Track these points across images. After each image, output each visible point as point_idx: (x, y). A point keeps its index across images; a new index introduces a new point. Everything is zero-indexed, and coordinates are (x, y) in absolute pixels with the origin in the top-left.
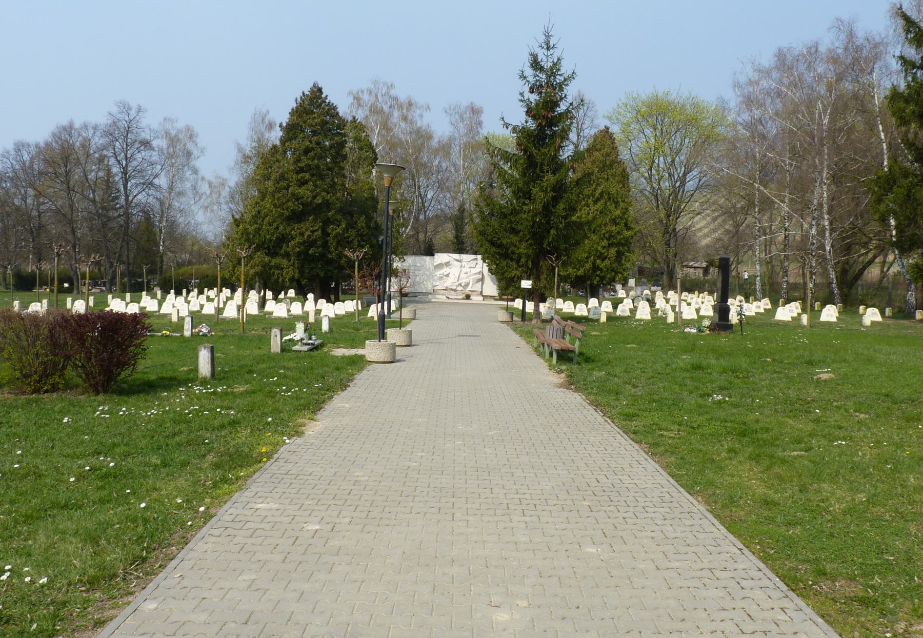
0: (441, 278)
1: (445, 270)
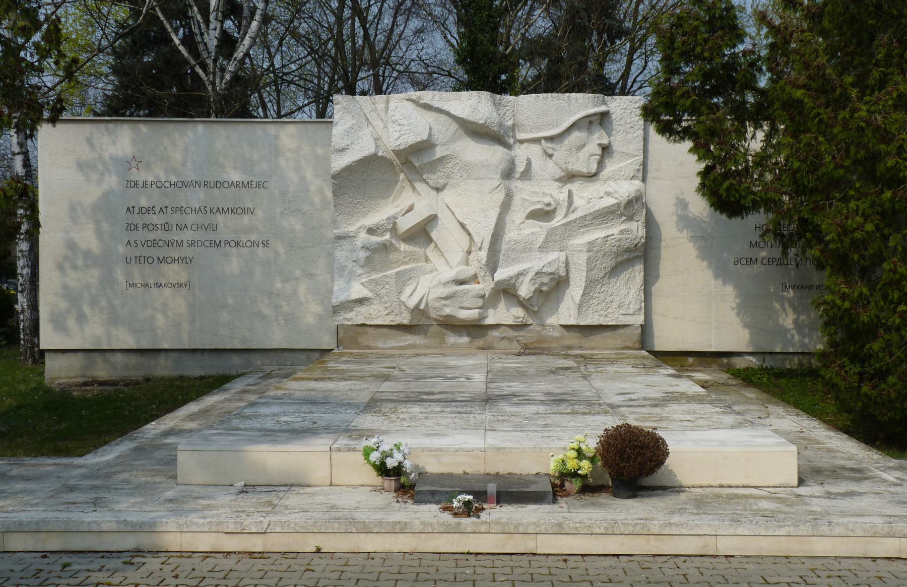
0: (378, 255)
1: (408, 203)
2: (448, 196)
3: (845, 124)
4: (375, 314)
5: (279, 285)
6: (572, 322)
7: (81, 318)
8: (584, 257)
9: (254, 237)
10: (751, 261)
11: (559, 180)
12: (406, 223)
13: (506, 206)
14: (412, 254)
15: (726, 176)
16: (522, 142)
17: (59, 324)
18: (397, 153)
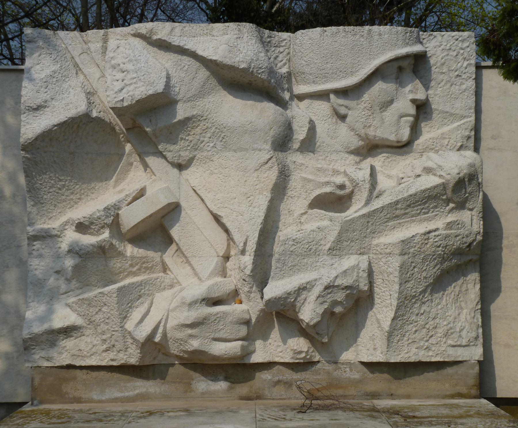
0: (91, 265)
1: (138, 186)
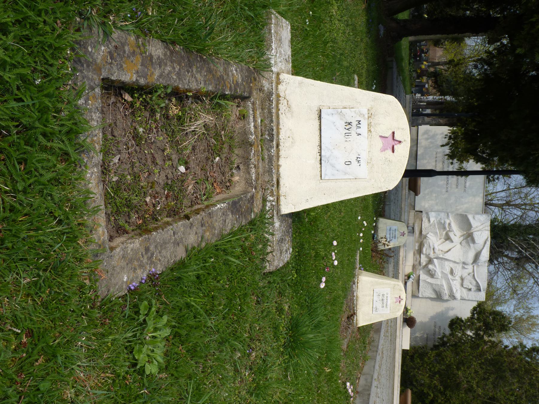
0: (442, 226)
1: (457, 234)
2: (459, 246)
3: (472, 359)
4: (425, 224)
5: (434, 195)
6: (421, 278)
7: (427, 139)
8: (439, 283)
9: (449, 188)
10: (435, 326)
11: (462, 276)
12: (451, 235)
13: (455, 262)
14: (442, 235)
15: (461, 326)
16: (473, 267)
17: (426, 132)
18: (472, 233)
